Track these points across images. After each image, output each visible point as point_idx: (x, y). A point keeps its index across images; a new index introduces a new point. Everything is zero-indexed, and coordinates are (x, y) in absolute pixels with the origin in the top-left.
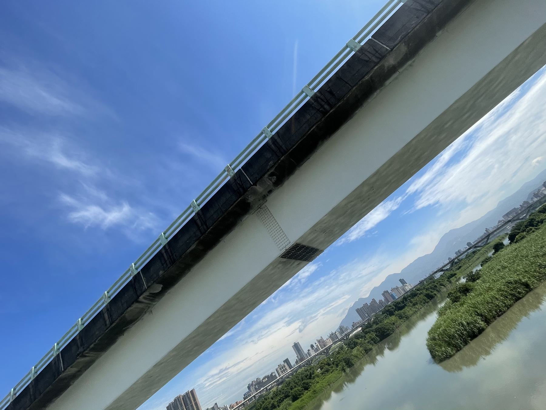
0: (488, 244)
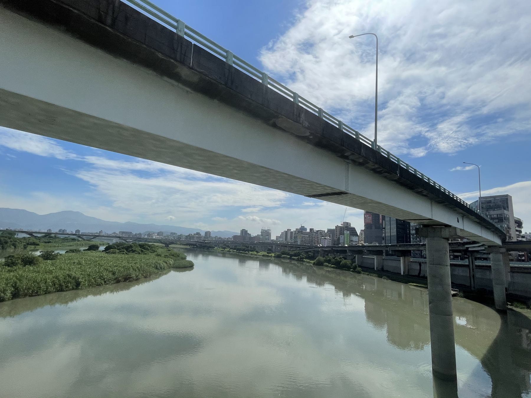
0: (90, 241)
